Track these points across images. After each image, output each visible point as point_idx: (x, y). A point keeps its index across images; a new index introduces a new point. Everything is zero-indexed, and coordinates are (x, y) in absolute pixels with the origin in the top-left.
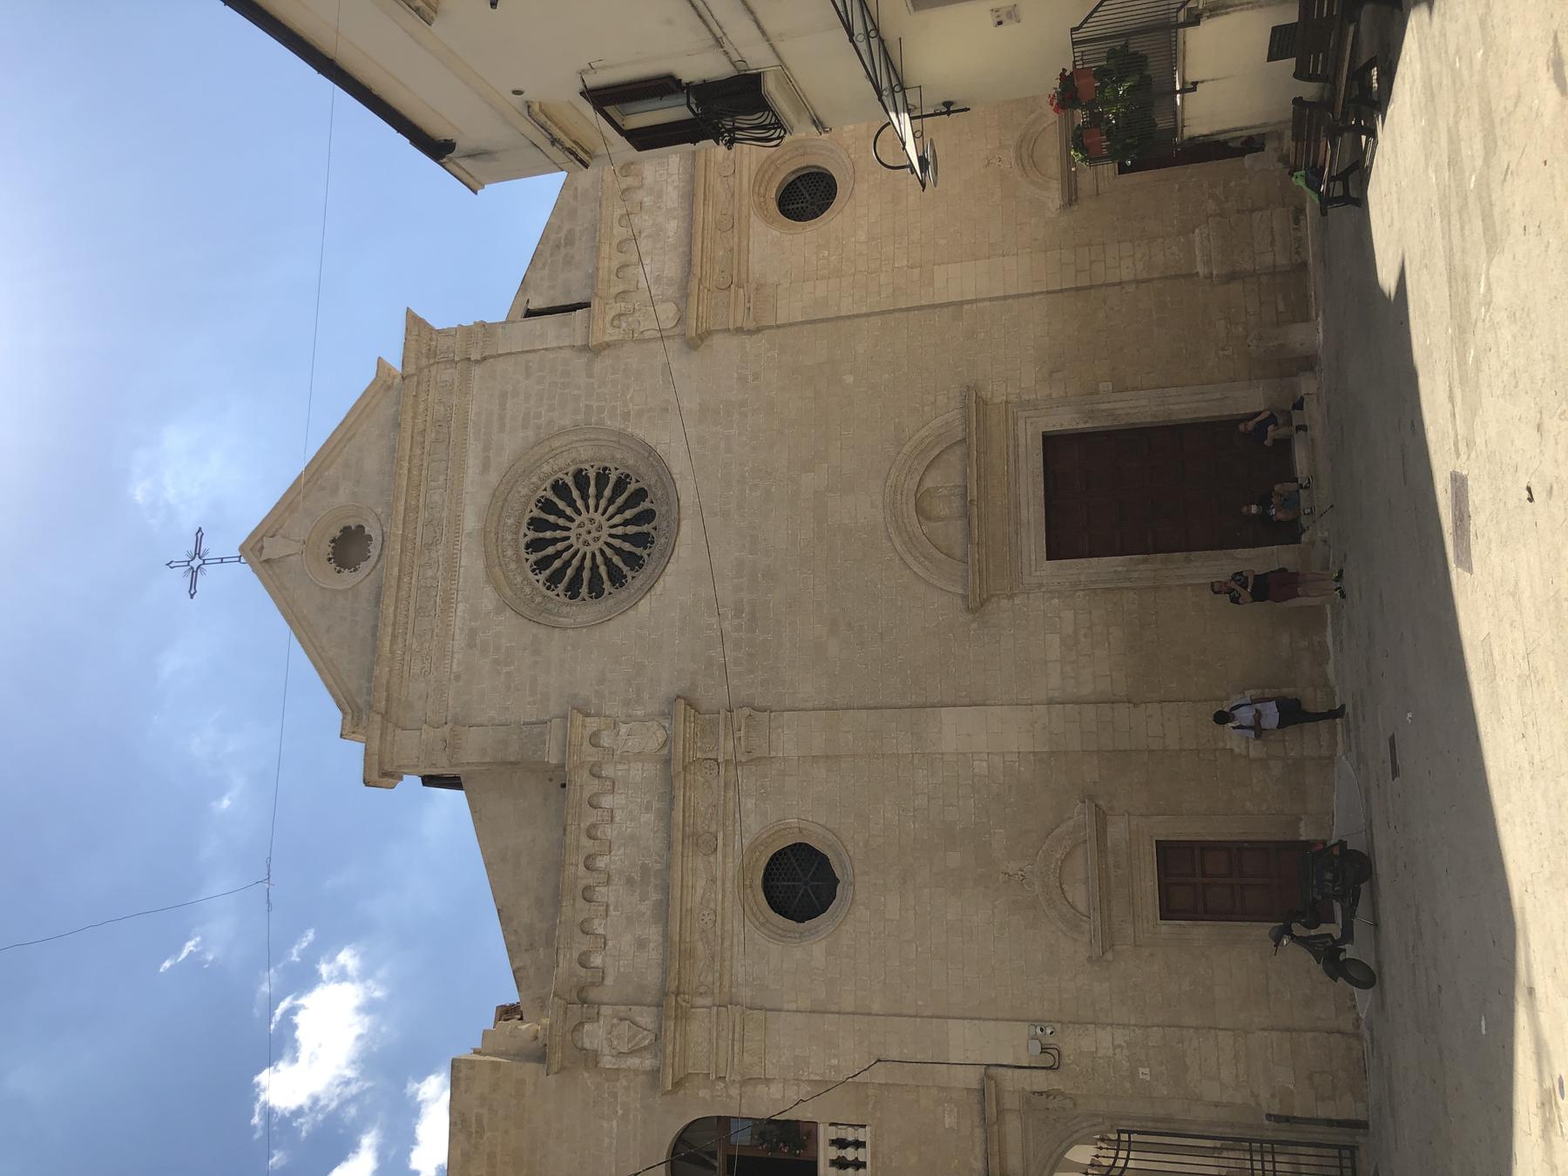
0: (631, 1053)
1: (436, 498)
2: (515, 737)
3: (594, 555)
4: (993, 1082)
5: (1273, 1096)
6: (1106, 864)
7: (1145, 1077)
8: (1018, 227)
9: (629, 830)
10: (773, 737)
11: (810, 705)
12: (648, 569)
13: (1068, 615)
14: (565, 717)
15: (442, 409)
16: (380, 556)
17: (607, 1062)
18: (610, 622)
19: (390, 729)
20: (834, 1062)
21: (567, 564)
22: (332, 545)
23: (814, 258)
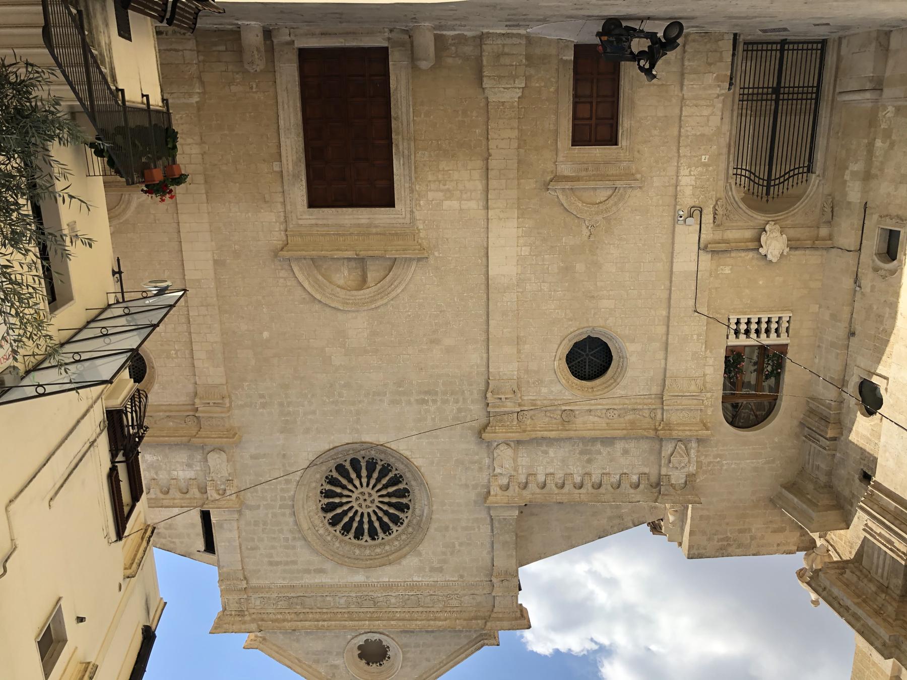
0: (688, 454)
1: (342, 601)
2: (501, 537)
3: (380, 496)
4: (709, 246)
5: (719, 86)
6: (586, 176)
7: (707, 159)
8: (157, 222)
9: (559, 463)
10: (505, 377)
11: (485, 355)
12: (392, 461)
13: (431, 195)
14: (489, 508)
15: (280, 603)
16: (381, 633)
17: (692, 469)
18: (429, 483)
19: (494, 615)
20: (695, 337)
21: (386, 513)
22: (371, 664)
23: (176, 360)
